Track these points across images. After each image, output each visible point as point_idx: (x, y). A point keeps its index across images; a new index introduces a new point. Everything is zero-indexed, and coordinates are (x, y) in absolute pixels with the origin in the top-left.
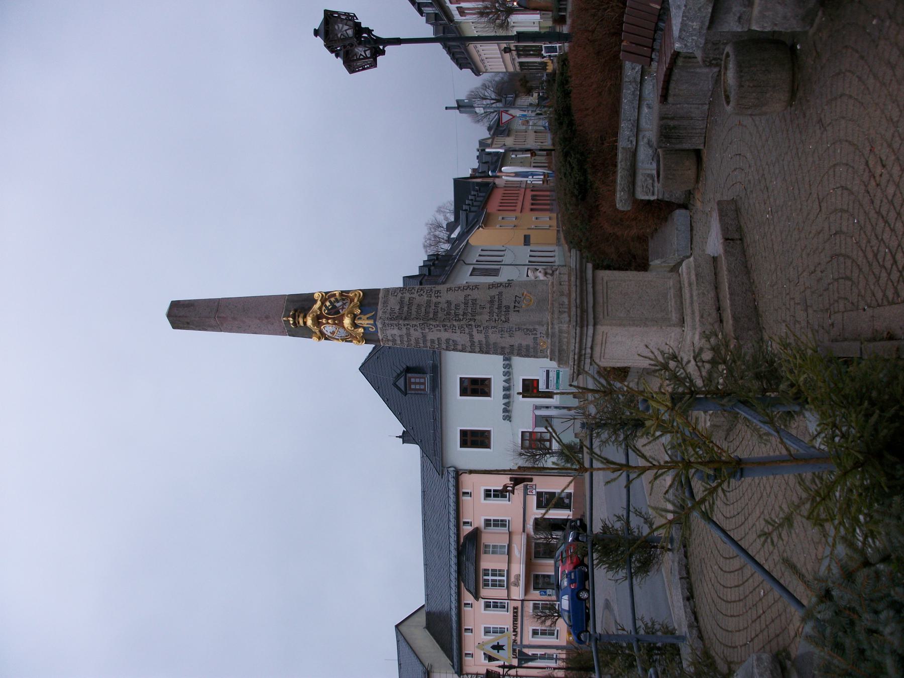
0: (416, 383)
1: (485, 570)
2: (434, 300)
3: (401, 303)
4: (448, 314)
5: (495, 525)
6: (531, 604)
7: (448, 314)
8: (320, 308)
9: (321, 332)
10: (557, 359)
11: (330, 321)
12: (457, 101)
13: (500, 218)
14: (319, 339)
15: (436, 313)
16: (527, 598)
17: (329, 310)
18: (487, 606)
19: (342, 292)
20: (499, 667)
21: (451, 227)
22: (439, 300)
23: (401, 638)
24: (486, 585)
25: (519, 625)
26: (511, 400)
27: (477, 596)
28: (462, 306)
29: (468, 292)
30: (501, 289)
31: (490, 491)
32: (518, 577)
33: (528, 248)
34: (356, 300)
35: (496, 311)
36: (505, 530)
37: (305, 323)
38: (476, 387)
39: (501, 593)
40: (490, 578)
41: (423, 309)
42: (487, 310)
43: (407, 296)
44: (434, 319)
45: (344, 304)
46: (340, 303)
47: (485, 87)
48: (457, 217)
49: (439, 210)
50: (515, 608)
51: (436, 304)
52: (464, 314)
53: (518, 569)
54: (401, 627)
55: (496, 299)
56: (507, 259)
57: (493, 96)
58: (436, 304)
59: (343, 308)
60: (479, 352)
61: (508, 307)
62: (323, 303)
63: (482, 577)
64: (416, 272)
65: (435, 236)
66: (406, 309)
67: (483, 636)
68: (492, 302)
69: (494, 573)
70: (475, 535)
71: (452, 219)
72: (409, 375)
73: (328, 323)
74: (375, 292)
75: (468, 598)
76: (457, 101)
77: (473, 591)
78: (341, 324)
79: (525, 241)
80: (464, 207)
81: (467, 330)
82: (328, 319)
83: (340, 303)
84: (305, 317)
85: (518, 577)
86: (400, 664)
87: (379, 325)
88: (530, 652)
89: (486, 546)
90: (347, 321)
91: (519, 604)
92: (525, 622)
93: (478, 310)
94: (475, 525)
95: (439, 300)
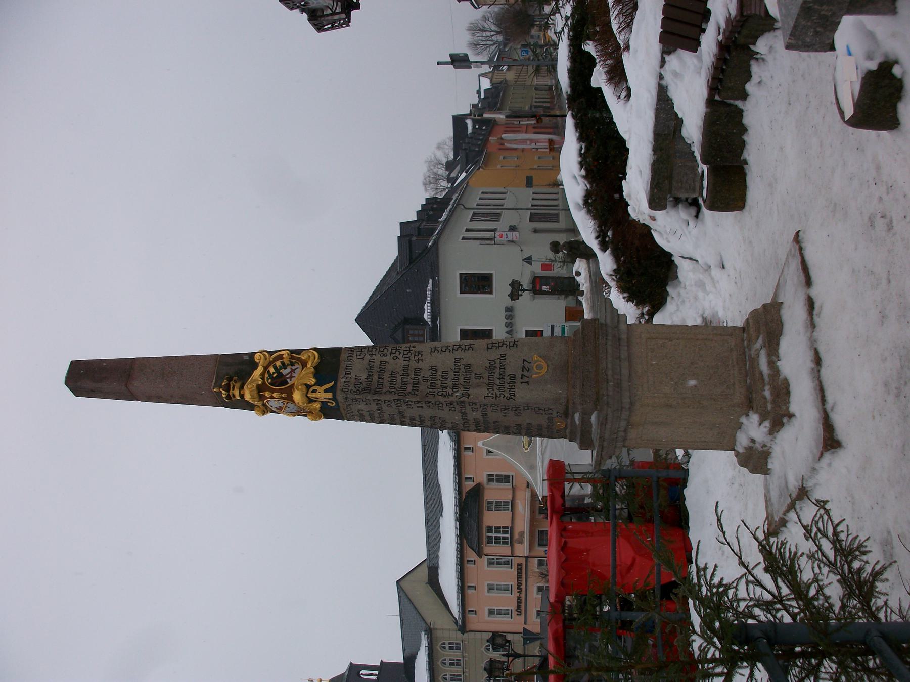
0: (414, 335)
1: (488, 527)
2: (413, 364)
3: (370, 368)
4: (433, 386)
5: (499, 481)
6: (536, 560)
7: (433, 386)
8: (262, 375)
9: (264, 405)
10: (578, 440)
11: (274, 395)
12: (451, 55)
13: (501, 158)
14: (264, 413)
15: (416, 384)
16: (533, 554)
17: (273, 378)
18: (491, 563)
19: (292, 351)
20: (504, 655)
21: (450, 166)
22: (421, 365)
23: (403, 597)
24: (490, 542)
25: (523, 583)
26: (514, 328)
27: (480, 554)
28: (452, 374)
29: (459, 354)
30: (503, 350)
31: (491, 527)
32: (522, 534)
33: (530, 191)
34: (309, 365)
35: (497, 382)
36: (509, 485)
37: (242, 396)
38: (478, 284)
39: (505, 549)
40: (493, 535)
41: (399, 380)
42: (486, 381)
43: (378, 358)
44: (413, 393)
45: (293, 371)
46: (288, 370)
47: (485, 19)
48: (456, 155)
49: (439, 147)
50: (519, 565)
51: (417, 371)
52: (455, 386)
53: (523, 525)
54: (402, 583)
55: (498, 365)
56: (508, 203)
57: (493, 28)
58: (417, 371)
59: (291, 378)
60: (475, 431)
61: (513, 377)
62: (266, 368)
63: (485, 535)
64: (414, 217)
65: (436, 174)
66: (375, 378)
67: (486, 568)
68: (491, 368)
69: (498, 529)
70: (477, 491)
71: (451, 156)
72: (407, 327)
73: (272, 397)
74: (335, 352)
75: (471, 555)
76: (451, 55)
77: (475, 548)
78: (290, 399)
79: (527, 183)
80: (464, 146)
81: (458, 408)
82: (273, 391)
83: (288, 370)
84: (242, 388)
85: (522, 534)
86: (401, 621)
87: (340, 397)
88: (507, 145)
89: (490, 503)
90: (297, 396)
91: (523, 561)
92: (530, 580)
93: (474, 381)
94: (477, 481)
95: (421, 365)
